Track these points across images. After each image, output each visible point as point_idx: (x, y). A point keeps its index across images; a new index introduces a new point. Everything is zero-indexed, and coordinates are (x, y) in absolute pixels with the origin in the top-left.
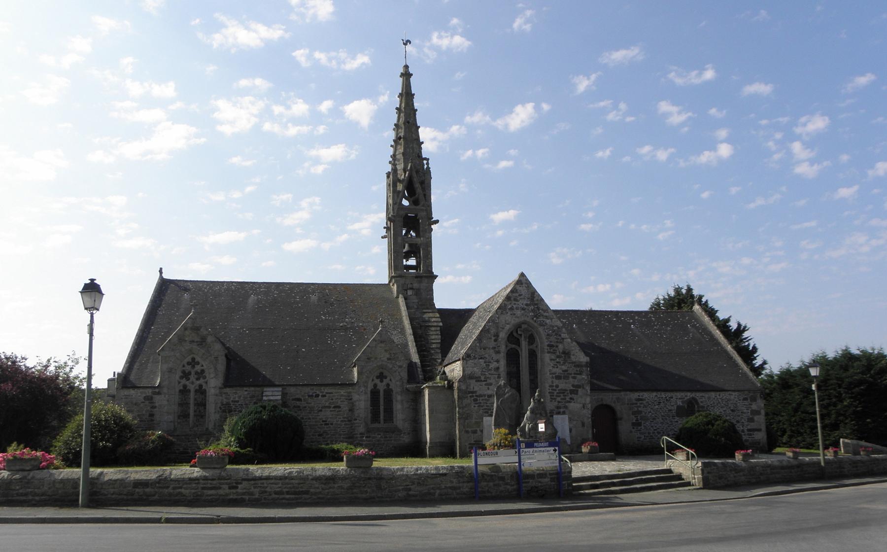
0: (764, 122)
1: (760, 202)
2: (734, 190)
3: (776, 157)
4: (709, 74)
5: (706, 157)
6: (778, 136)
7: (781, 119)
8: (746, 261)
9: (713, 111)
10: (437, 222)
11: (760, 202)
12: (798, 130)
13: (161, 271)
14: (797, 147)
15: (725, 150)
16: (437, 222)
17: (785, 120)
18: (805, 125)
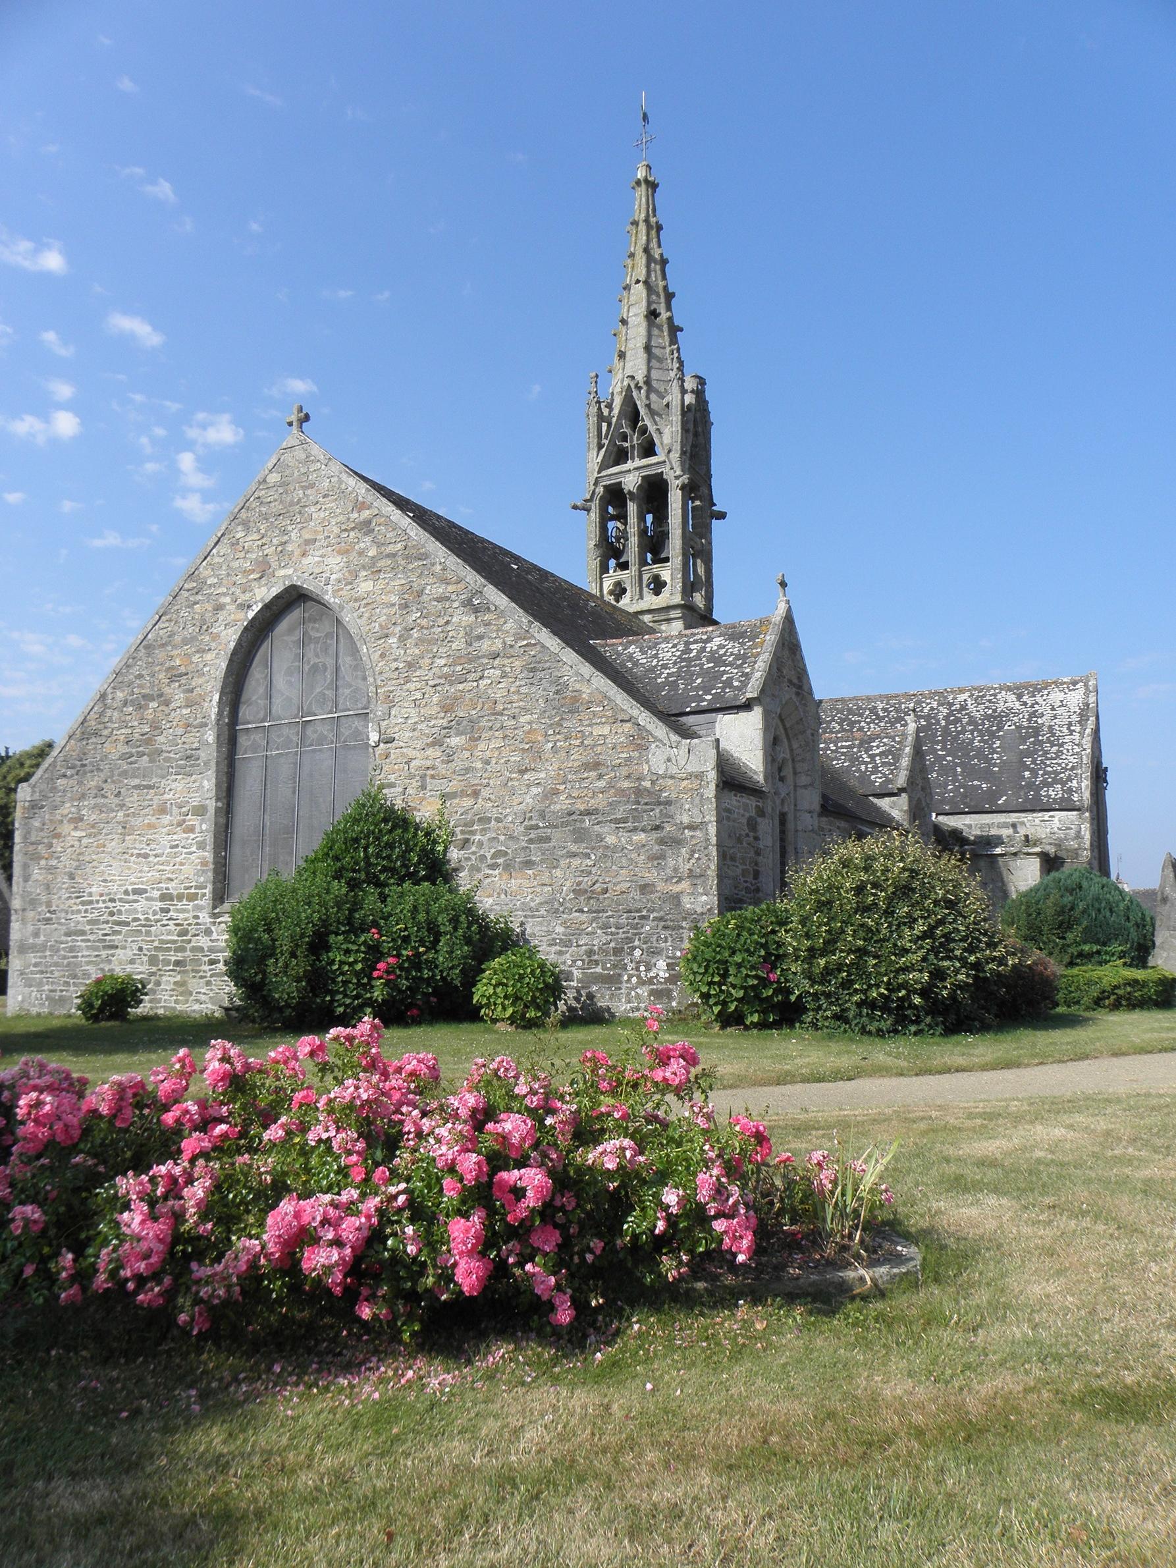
0: (138, 398)
1: (112, 539)
2: (67, 506)
3: (150, 467)
4: (53, 261)
5: (25, 426)
6: (160, 432)
7: (168, 403)
8: (74, 641)
9: (50, 336)
10: (722, 516)
11: (112, 539)
12: (192, 433)
13: (575, 507)
14: (187, 461)
15: (66, 424)
16: (722, 516)
17: (173, 407)
18: (204, 427)
